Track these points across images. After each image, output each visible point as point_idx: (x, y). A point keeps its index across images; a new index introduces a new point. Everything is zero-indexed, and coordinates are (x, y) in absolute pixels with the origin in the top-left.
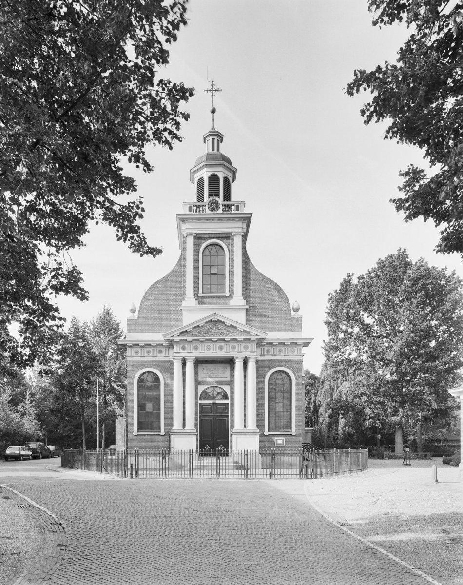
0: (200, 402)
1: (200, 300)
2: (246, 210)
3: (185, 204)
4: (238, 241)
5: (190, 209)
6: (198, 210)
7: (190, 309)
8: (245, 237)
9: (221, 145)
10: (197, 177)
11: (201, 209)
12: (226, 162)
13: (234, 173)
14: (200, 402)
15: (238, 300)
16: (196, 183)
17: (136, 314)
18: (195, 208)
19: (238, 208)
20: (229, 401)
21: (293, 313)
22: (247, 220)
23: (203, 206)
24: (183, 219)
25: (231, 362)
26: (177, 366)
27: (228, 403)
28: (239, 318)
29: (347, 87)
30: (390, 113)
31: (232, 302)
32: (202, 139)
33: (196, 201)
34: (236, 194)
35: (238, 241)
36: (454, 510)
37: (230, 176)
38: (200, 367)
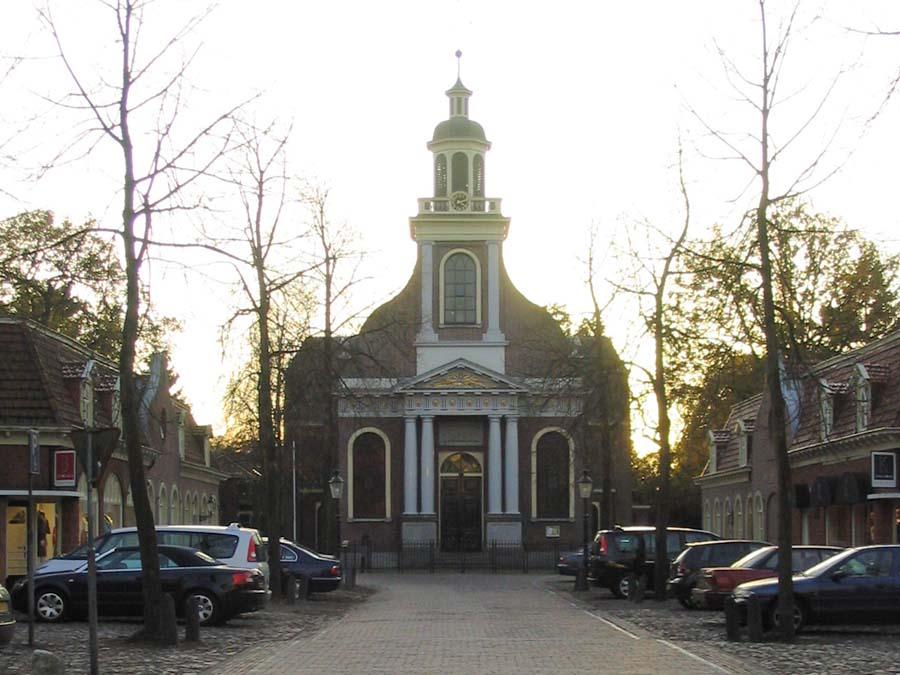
25: (484, 421)
27: (480, 477)
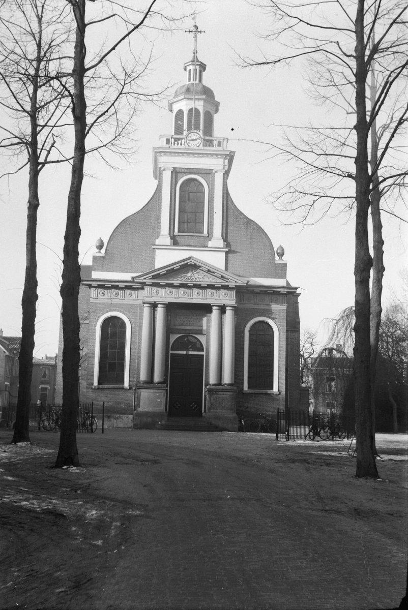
0: (171, 352)
1: (175, 242)
2: (230, 147)
3: (161, 137)
4: (218, 179)
5: (168, 141)
6: (176, 143)
7: (163, 247)
8: (227, 174)
9: (204, 74)
10: (176, 107)
11: (180, 142)
12: (208, 93)
13: (217, 106)
14: (171, 352)
15: (217, 241)
16: (174, 113)
17: (103, 251)
18: (173, 140)
19: (219, 144)
20: (204, 353)
21: (277, 258)
22: (230, 157)
23: (182, 139)
24: (157, 153)
26: (146, 310)
27: (203, 355)
28: (217, 260)
29: (212, 240)
30: (76, 421)
31: (210, 244)
32: (183, 67)
33: (173, 134)
34: (220, 127)
35: (218, 179)
36: (404, 447)
37: (211, 109)
38: (165, 391)
